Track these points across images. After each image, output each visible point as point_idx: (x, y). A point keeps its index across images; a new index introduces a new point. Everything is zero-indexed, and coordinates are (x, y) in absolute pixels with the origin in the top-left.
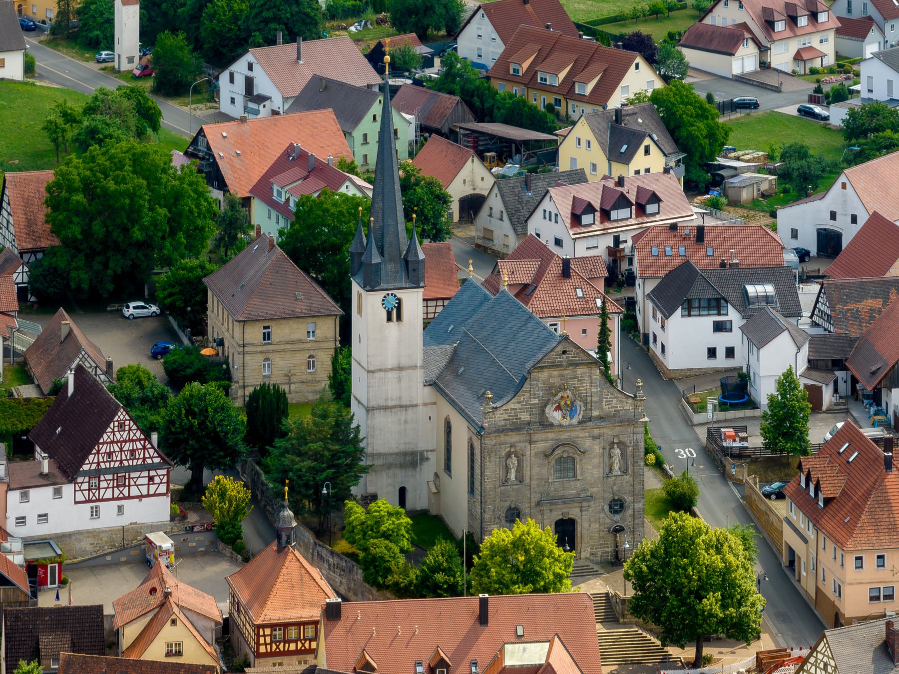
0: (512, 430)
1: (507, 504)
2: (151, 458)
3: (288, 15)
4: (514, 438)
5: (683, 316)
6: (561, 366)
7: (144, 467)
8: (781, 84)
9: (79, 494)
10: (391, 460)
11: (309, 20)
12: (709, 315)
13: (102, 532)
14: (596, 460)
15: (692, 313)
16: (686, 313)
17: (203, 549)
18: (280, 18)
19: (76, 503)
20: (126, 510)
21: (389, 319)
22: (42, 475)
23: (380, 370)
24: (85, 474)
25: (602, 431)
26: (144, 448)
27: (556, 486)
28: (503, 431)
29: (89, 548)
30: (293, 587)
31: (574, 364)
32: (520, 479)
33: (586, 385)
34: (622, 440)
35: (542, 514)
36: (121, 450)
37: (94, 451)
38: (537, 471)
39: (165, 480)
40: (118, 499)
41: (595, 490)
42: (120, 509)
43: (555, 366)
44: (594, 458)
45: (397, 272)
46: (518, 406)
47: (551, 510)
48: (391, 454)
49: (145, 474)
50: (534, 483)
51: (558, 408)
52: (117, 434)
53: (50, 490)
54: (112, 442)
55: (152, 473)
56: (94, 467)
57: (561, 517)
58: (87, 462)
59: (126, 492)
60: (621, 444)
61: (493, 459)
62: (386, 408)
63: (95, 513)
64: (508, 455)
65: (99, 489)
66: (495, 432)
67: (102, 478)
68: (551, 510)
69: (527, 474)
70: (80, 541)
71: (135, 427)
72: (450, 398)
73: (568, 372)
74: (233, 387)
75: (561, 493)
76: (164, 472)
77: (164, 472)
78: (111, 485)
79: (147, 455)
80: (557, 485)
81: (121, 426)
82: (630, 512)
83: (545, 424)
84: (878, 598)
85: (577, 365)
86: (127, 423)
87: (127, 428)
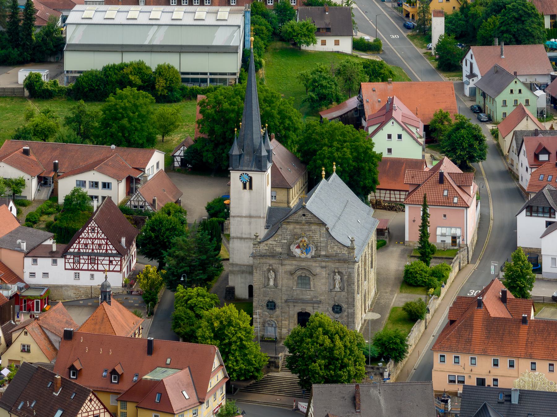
0: (269, 256)
1: (267, 299)
2: (111, 250)
3: (515, 30)
4: (272, 261)
6: (301, 223)
7: (106, 255)
9: (67, 265)
10: (244, 268)
11: (527, 34)
12: (544, 217)
13: (81, 287)
15: (533, 214)
16: (529, 214)
17: (137, 305)
18: (511, 31)
19: (66, 269)
20: (95, 276)
21: (245, 187)
23: (238, 216)
24: (71, 254)
25: (327, 264)
26: (107, 244)
27: (297, 292)
28: (264, 256)
29: (73, 295)
30: (96, 324)
31: (309, 223)
32: (276, 285)
33: (317, 236)
34: (340, 270)
35: (289, 308)
36: (93, 243)
37: (76, 242)
38: (285, 282)
39: (119, 263)
40: (91, 270)
41: (323, 298)
42: (92, 276)
43: (297, 222)
44: (322, 279)
45: (250, 161)
46: (274, 243)
47: (294, 306)
48: (244, 265)
49: (107, 258)
50: (284, 288)
51: (298, 247)
52: (90, 234)
53: (50, 260)
54: (88, 238)
55: (112, 259)
56: (76, 250)
57: (300, 311)
58: (72, 247)
59: (95, 267)
60: (339, 273)
61: (258, 271)
62: (241, 238)
63: (77, 276)
64: (269, 270)
65: (80, 263)
66: (258, 256)
67: (81, 257)
68: (294, 306)
69: (280, 283)
70: (68, 291)
71: (101, 232)
73: (306, 227)
74: (226, 222)
75: (301, 297)
76: (119, 259)
77: (119, 259)
78: (87, 262)
79: (108, 248)
80: (298, 292)
81: (93, 230)
82: (346, 313)
83: (290, 255)
84: (454, 382)
85: (311, 223)
86: (96, 228)
87: (96, 231)
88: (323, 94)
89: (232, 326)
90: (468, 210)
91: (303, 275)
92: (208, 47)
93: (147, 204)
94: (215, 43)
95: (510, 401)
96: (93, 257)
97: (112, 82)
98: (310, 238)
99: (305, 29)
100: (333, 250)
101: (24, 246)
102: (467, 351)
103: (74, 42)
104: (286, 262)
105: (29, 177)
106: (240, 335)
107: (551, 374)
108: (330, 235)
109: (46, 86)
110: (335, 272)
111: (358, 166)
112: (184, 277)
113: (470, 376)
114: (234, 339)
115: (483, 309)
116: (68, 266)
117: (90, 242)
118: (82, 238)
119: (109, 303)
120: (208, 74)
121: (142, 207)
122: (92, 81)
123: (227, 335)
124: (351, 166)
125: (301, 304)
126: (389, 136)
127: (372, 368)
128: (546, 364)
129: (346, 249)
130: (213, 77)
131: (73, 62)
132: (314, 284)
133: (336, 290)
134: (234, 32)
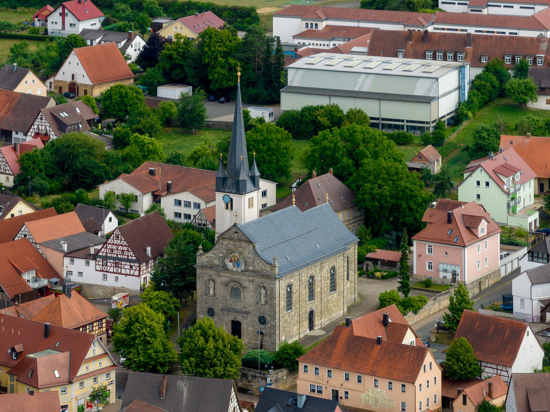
0: (208, 267)
1: (208, 306)
2: (132, 256)
4: (211, 272)
5: (529, 260)
6: (233, 239)
7: (127, 260)
8: (73, 76)
12: (538, 262)
13: (108, 288)
14: (251, 293)
19: (96, 270)
21: (227, 208)
22: (90, 255)
25: (255, 278)
26: (128, 250)
27: (231, 302)
29: (101, 294)
31: (240, 240)
32: (214, 294)
36: (117, 249)
38: (223, 292)
39: (138, 269)
40: (116, 273)
41: (250, 309)
42: (117, 278)
43: (231, 239)
46: (213, 256)
49: (128, 263)
51: (231, 261)
53: (83, 261)
54: (113, 244)
55: (132, 264)
56: (104, 254)
57: (233, 319)
59: (119, 270)
60: (264, 288)
61: (200, 280)
63: (105, 278)
64: (209, 280)
67: (108, 261)
69: (217, 292)
72: (304, 265)
75: (233, 306)
80: (231, 302)
82: (269, 325)
86: (120, 236)
88: (480, 145)
89: (139, 323)
90: (466, 249)
91: (235, 287)
92: (408, 96)
93: (208, 223)
94: (416, 93)
95: (296, 405)
96: (117, 262)
97: (305, 121)
98: (241, 253)
99: (523, 87)
100: (260, 266)
101: (65, 247)
102: (325, 364)
103: (294, 84)
104: (222, 274)
105: (141, 194)
106: (144, 331)
107: (390, 392)
108: (257, 253)
109: (252, 122)
110: (261, 287)
111: (397, 203)
112: (164, 283)
113: (326, 387)
114: (139, 334)
115: (349, 328)
116: (98, 268)
117: (115, 248)
118: (109, 244)
119: (69, 296)
120: (405, 121)
121: (204, 225)
122: (289, 120)
123: (133, 331)
124: (389, 202)
125: (233, 313)
126: (478, 183)
127: (260, 373)
128: (387, 382)
129: (269, 266)
130: (409, 124)
131: (290, 103)
132: (244, 296)
133: (261, 303)
134: (433, 84)
